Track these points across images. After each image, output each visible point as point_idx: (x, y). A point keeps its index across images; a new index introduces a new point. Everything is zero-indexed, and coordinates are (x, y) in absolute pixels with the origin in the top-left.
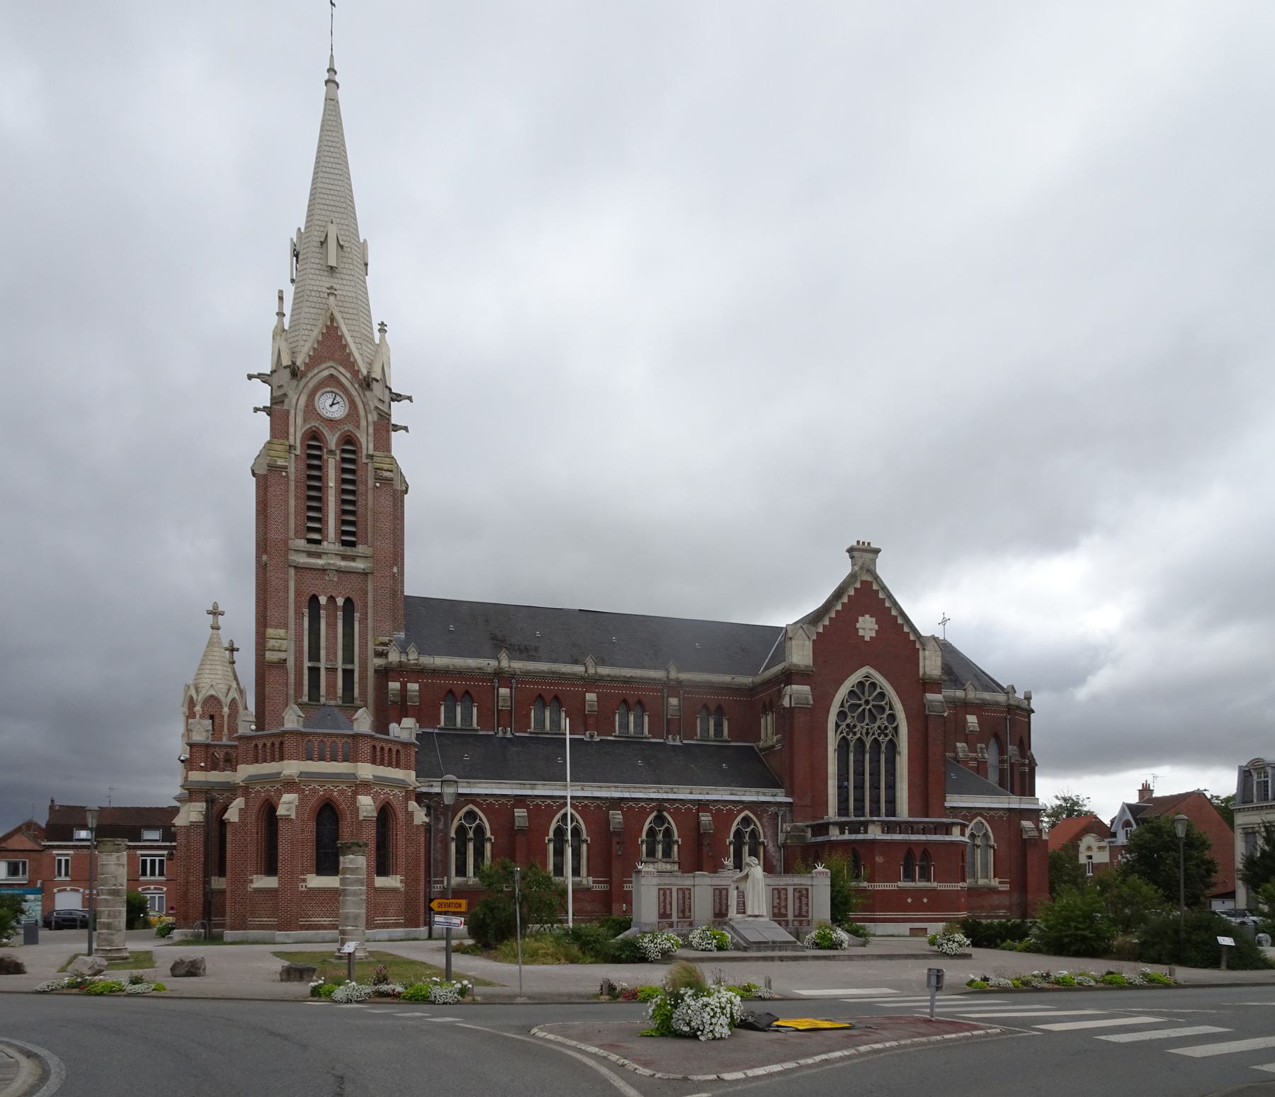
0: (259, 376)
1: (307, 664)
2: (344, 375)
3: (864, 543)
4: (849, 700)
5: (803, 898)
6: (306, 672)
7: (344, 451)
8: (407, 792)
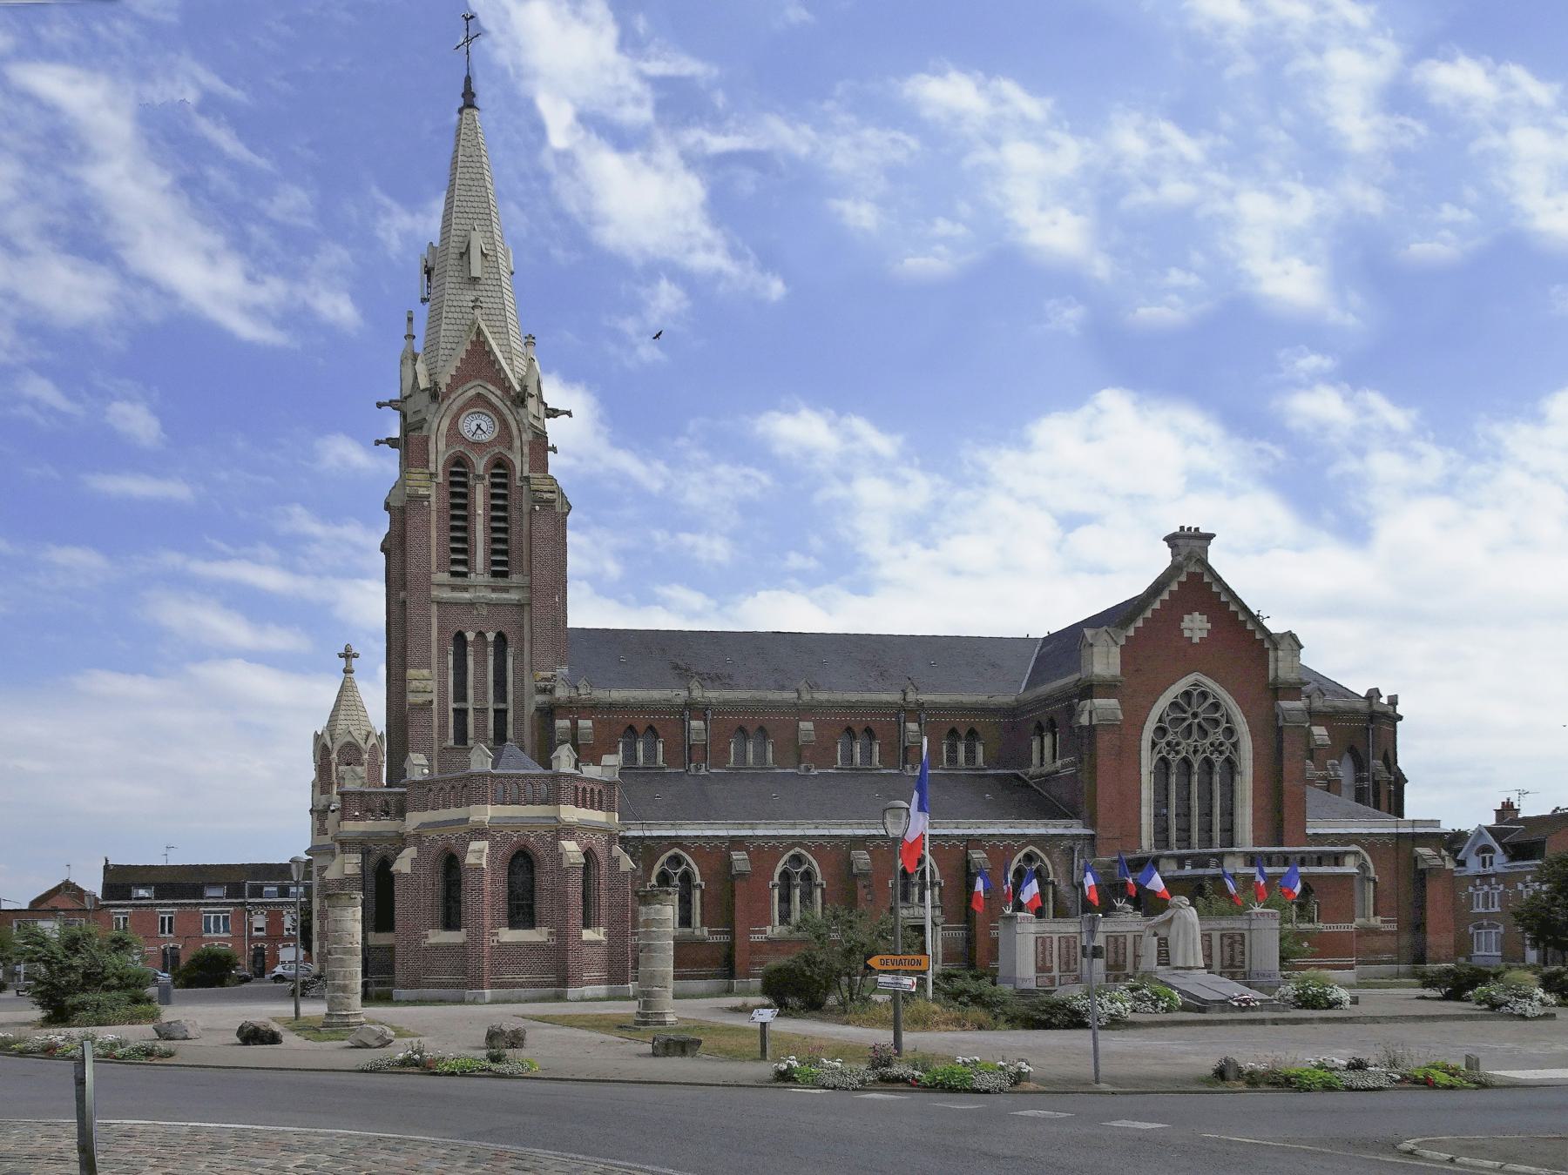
0: (391, 403)
1: (452, 705)
2: (493, 393)
3: (1189, 529)
4: (1170, 713)
5: (1237, 946)
6: (451, 714)
7: (494, 475)
8: (610, 835)
